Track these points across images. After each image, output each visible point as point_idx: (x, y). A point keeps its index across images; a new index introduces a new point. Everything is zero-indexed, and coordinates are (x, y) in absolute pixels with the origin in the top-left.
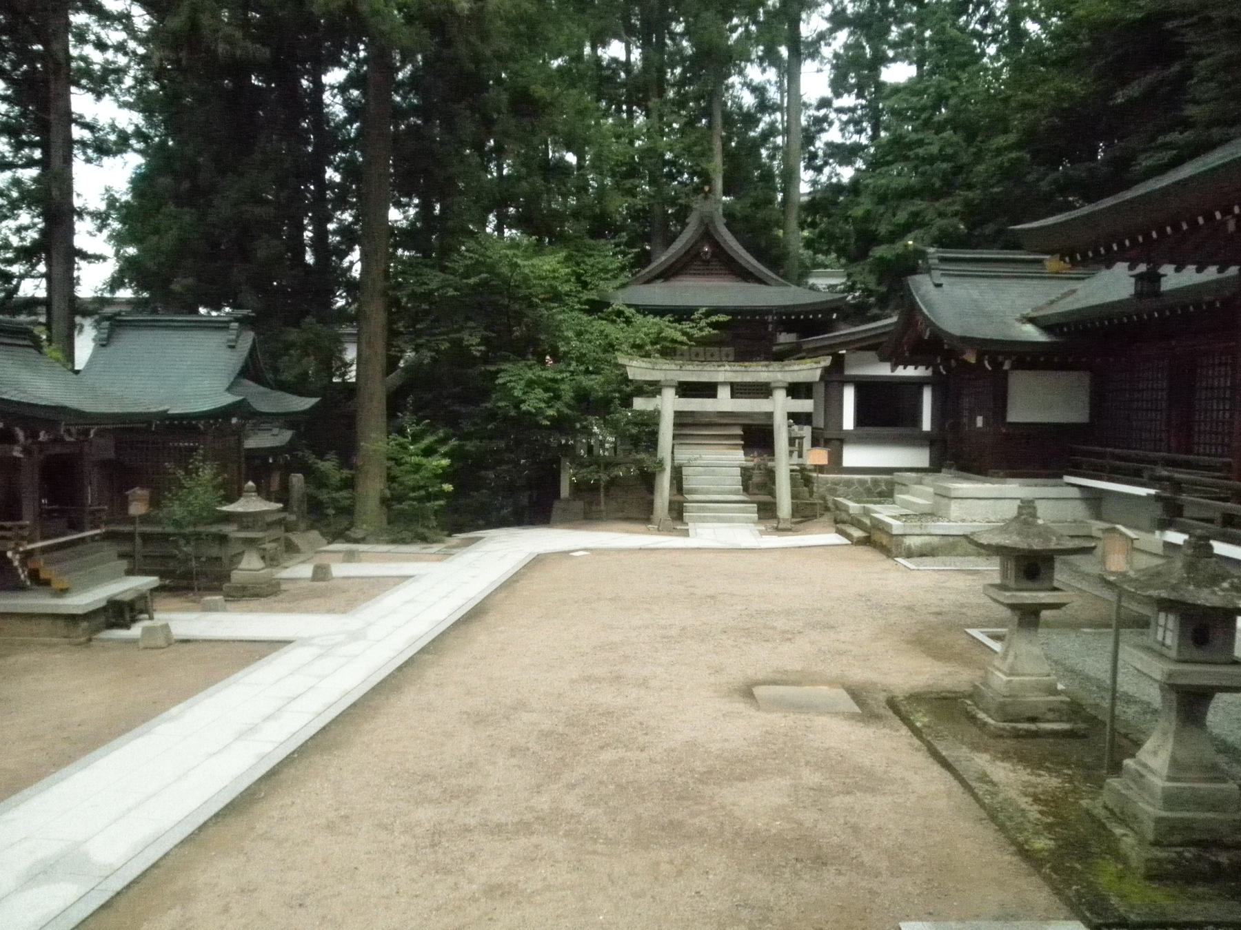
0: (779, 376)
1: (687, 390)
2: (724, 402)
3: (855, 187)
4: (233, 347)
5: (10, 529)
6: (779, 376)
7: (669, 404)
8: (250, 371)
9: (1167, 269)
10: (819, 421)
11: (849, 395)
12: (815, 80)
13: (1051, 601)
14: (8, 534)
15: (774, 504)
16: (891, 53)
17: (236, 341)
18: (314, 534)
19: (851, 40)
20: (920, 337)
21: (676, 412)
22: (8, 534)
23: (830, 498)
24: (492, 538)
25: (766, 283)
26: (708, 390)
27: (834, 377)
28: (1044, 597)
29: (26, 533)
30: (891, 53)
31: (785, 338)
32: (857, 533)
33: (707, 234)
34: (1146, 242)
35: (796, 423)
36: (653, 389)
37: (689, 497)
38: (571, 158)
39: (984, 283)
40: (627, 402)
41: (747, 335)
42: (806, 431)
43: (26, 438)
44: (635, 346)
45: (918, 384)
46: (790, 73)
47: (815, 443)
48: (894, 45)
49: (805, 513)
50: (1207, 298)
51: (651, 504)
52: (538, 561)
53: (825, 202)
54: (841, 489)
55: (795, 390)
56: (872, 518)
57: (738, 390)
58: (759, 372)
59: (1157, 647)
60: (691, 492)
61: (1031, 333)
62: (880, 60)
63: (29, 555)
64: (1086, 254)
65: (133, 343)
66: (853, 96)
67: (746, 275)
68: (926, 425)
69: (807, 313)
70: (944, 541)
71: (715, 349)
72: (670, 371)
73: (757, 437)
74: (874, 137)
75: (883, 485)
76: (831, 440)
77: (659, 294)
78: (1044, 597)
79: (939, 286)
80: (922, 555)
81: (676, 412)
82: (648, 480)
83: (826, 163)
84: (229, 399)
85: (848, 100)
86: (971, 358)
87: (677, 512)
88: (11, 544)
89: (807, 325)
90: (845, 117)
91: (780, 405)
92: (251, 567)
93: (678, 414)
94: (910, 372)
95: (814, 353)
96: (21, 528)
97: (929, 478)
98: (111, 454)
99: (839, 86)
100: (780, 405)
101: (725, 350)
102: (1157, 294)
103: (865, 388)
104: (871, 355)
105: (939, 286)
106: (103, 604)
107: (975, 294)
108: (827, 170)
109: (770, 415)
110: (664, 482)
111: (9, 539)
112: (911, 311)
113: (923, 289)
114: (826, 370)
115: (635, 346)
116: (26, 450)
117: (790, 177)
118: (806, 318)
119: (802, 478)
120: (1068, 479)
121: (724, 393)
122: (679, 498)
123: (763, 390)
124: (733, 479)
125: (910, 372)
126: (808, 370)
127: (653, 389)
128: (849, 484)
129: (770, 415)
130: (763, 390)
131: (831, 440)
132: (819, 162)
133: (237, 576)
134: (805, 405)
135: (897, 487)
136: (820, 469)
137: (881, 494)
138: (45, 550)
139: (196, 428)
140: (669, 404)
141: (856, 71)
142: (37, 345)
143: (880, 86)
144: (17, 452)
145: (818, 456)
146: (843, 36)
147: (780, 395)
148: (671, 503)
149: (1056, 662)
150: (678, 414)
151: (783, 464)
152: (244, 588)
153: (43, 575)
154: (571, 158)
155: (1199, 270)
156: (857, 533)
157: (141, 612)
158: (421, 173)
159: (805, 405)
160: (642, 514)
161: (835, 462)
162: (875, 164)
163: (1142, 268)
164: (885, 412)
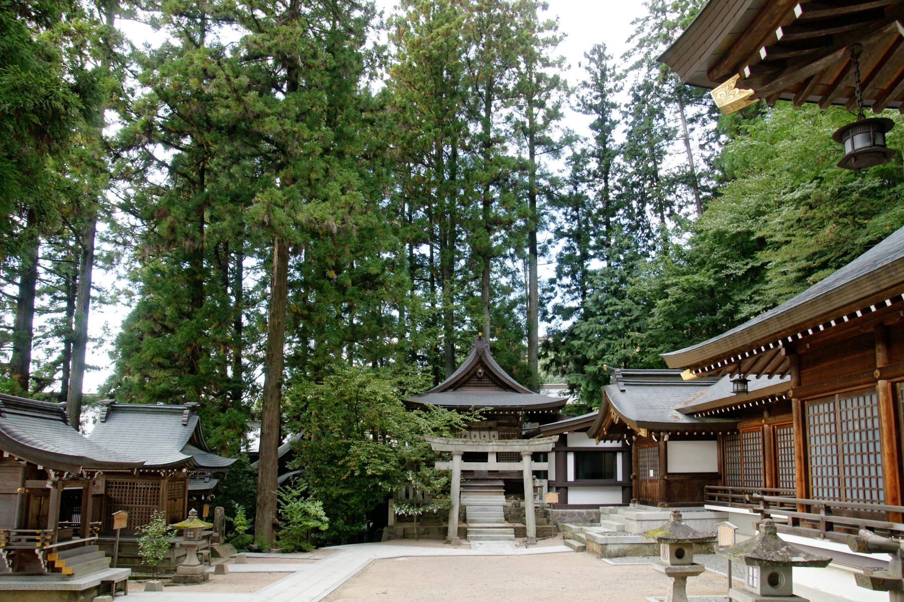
0: (527, 448)
1: (468, 457)
2: (492, 464)
3: (571, 334)
4: (185, 425)
5: (39, 535)
6: (527, 448)
7: (457, 466)
8: (195, 441)
9: (751, 377)
10: (552, 476)
11: (571, 458)
12: (546, 270)
13: (692, 571)
14: (38, 538)
15: (525, 529)
16: (591, 253)
17: (187, 421)
18: (229, 546)
19: (567, 245)
20: (613, 423)
21: (462, 471)
22: (38, 538)
23: (560, 524)
24: (344, 550)
26: (482, 457)
27: (562, 447)
28: (688, 569)
29: (49, 537)
30: (591, 253)
31: (529, 426)
32: (577, 544)
33: (480, 361)
35: (538, 477)
36: (446, 456)
37: (471, 525)
38: (395, 313)
39: (651, 389)
40: (430, 464)
41: (504, 422)
42: (544, 483)
43: (56, 476)
44: (435, 429)
45: (613, 452)
46: (531, 265)
47: (549, 489)
48: (594, 248)
49: (542, 534)
51: (446, 529)
52: (374, 562)
53: (556, 342)
54: (567, 519)
55: (537, 457)
56: (587, 535)
58: (514, 446)
59: (748, 588)
60: (472, 521)
61: (683, 419)
62: (585, 256)
63: (50, 551)
64: (710, 370)
65: (121, 422)
66: (570, 278)
68: (620, 478)
69: (543, 410)
70: (631, 548)
71: (486, 433)
72: (459, 446)
73: (513, 487)
75: (593, 514)
76: (562, 488)
77: (451, 398)
78: (688, 569)
79: (623, 391)
80: (617, 556)
81: (462, 471)
82: (444, 515)
83: (553, 318)
84: (183, 457)
85: (567, 280)
86: (643, 433)
87: (463, 533)
88: (39, 544)
89: (545, 415)
90: (565, 290)
91: (527, 466)
92: (192, 564)
93: (464, 473)
94: (608, 444)
95: (548, 433)
96: (46, 534)
97: (621, 510)
98: (102, 491)
99: (560, 273)
100: (527, 466)
101: (492, 433)
102: (746, 391)
103: (580, 454)
105: (623, 391)
106: (99, 583)
107: (645, 395)
108: (554, 322)
109: (521, 473)
110: (455, 515)
111: (38, 541)
112: (607, 409)
113: (614, 393)
115: (435, 429)
116: (55, 484)
117: (532, 327)
119: (542, 513)
120: (707, 507)
121: (492, 458)
122: (464, 525)
123: (516, 457)
124: (500, 513)
125: (608, 444)
126: (545, 444)
127: (446, 456)
128: (573, 515)
129: (521, 473)
130: (516, 457)
131: (562, 488)
132: (550, 316)
133: (182, 569)
134: (541, 466)
135: (602, 516)
136: (554, 506)
137: (592, 521)
138: (60, 549)
139: (159, 474)
140: (457, 466)
141: (572, 264)
142: (65, 421)
143: (585, 273)
144: (49, 485)
145: (552, 497)
146: (563, 242)
148: (459, 528)
150: (464, 473)
151: (529, 504)
152: (186, 577)
153: (57, 565)
154: (395, 313)
155: (781, 378)
156: (577, 544)
157: (120, 590)
158: (304, 320)
159: (541, 466)
160: (442, 536)
161: (563, 502)
162: (585, 317)
163: (737, 377)
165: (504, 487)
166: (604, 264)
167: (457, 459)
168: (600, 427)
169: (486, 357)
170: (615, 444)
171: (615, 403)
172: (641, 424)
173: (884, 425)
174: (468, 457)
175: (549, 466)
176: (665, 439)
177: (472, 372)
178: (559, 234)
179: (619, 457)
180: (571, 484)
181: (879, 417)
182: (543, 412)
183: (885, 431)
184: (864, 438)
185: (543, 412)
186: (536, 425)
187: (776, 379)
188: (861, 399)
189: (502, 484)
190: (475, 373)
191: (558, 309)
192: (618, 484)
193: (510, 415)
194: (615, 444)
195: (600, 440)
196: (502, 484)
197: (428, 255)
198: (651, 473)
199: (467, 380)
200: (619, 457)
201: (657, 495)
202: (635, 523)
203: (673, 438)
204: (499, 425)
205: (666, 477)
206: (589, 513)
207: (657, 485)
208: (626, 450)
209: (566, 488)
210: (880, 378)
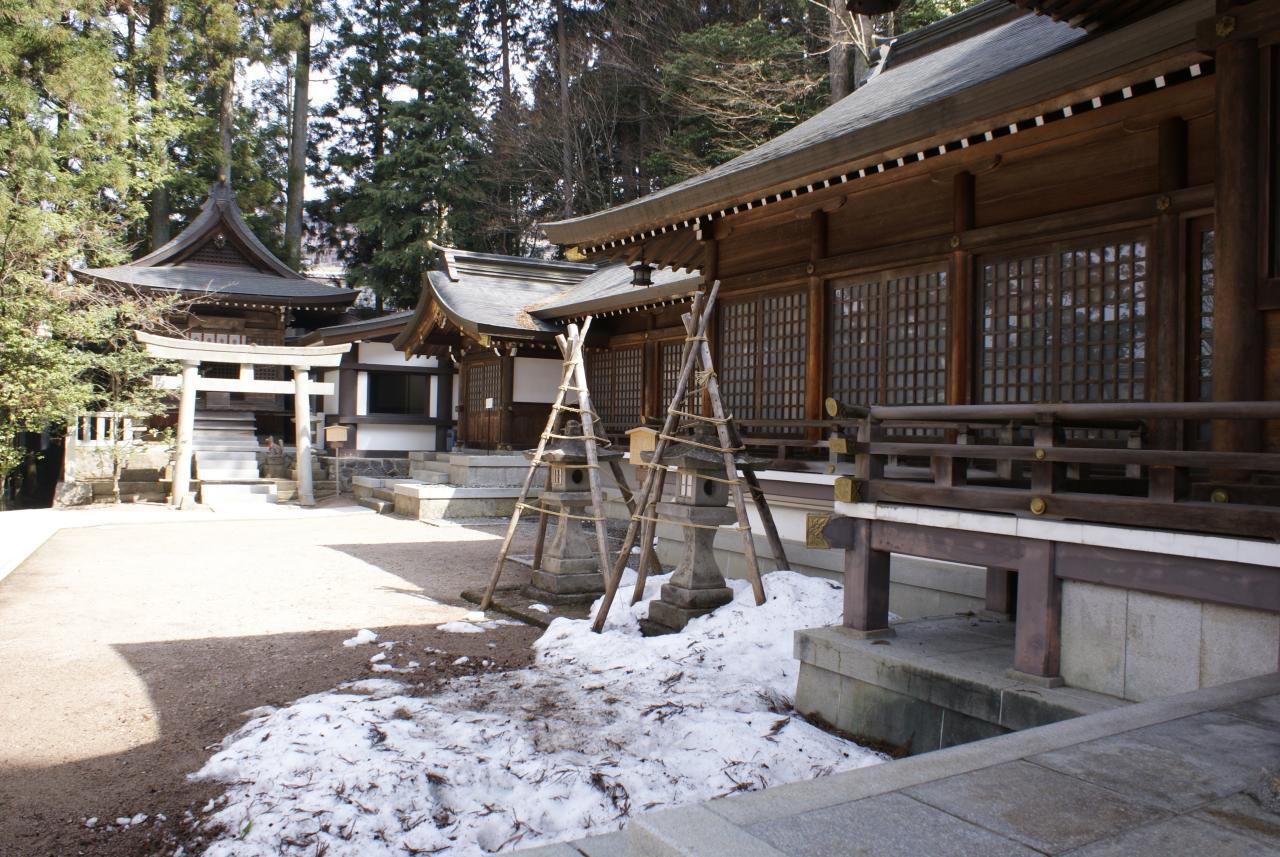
1: (210, 369)
2: (247, 383)
11: (363, 382)
25: (281, 276)
26: (231, 371)
27: (351, 365)
34: (644, 249)
45: (425, 374)
50: (675, 297)
55: (318, 374)
57: (263, 372)
67: (260, 266)
68: (433, 412)
71: (224, 336)
74: (377, 151)
86: (484, 341)
90: (349, 128)
93: (201, 395)
99: (345, 96)
100: (303, 389)
104: (389, 346)
114: (346, 357)
118: (320, 311)
121: (247, 374)
123: (288, 373)
126: (330, 355)
130: (288, 373)
140: (191, 384)
141: (362, 84)
143: (383, 101)
146: (352, 52)
147: (303, 378)
149: (248, 818)
155: (689, 272)
162: (378, 177)
164: (394, 397)
165: (255, 424)
166: (414, 94)
167: (192, 373)
168: (414, 333)
169: (231, 216)
170: (431, 362)
171: (444, 298)
172: (484, 328)
173: (812, 331)
174: (210, 369)
175: (328, 388)
176: (512, 354)
177: (207, 238)
178: (347, 36)
179: (434, 382)
180: (362, 419)
181: (808, 321)
182: (303, 309)
183: (812, 338)
184: (788, 346)
185: (303, 309)
186: (167, 366)
187: (682, 274)
188: (789, 299)
189: (252, 418)
190: (212, 240)
191: (338, 158)
192: (431, 422)
193: (267, 311)
194: (431, 362)
195: (412, 354)
196: (252, 418)
197: (125, 32)
198: (489, 403)
199: (198, 251)
200: (434, 382)
201: (495, 433)
202: (468, 471)
203: (522, 353)
204: (248, 325)
205: (510, 408)
206: (389, 462)
207: (496, 418)
208: (446, 372)
209: (355, 425)
210: (812, 275)
